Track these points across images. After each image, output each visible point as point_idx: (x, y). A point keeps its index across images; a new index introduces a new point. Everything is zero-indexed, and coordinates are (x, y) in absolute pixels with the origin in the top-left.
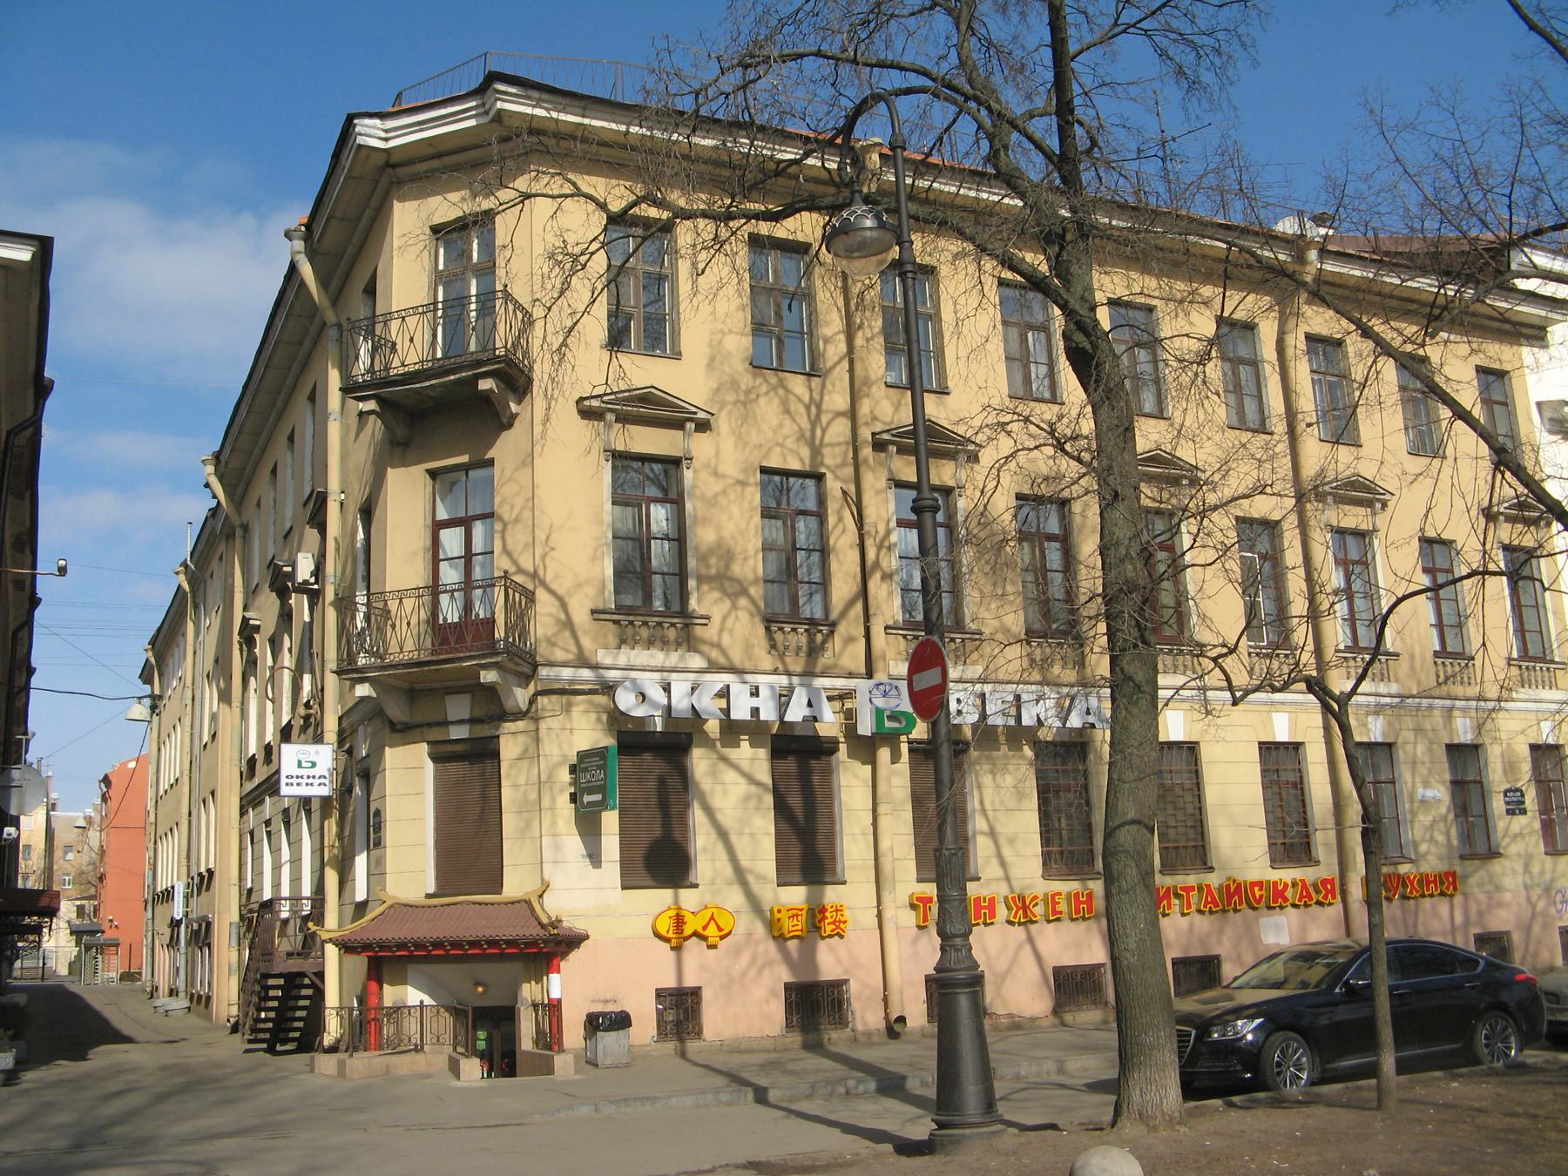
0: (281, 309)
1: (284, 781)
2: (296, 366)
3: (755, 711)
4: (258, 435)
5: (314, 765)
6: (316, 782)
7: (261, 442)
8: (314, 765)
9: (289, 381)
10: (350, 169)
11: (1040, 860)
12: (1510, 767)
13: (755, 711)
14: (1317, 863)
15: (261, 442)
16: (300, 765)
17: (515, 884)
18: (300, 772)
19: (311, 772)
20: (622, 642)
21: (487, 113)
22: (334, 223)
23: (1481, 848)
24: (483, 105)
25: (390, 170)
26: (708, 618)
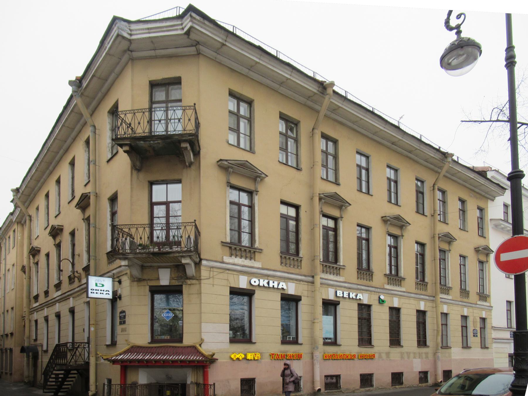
0: (56, 128)
1: (90, 291)
2: (61, 152)
3: (273, 286)
4: (39, 181)
5: (103, 285)
6: (105, 293)
7: (39, 185)
8: (103, 285)
9: (57, 158)
10: (110, 48)
11: (357, 340)
12: (474, 322)
13: (273, 286)
14: (428, 347)
15: (39, 185)
16: (96, 285)
17: (188, 340)
18: (97, 288)
19: (102, 288)
20: (231, 255)
21: (183, 29)
22: (95, 79)
23: (291, 338)
24: (182, 24)
25: (130, 52)
26: (262, 250)
